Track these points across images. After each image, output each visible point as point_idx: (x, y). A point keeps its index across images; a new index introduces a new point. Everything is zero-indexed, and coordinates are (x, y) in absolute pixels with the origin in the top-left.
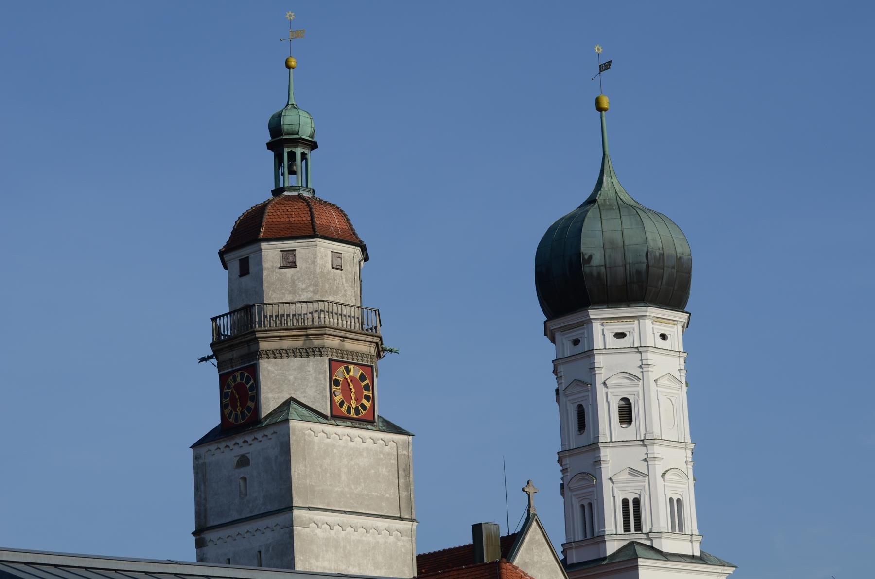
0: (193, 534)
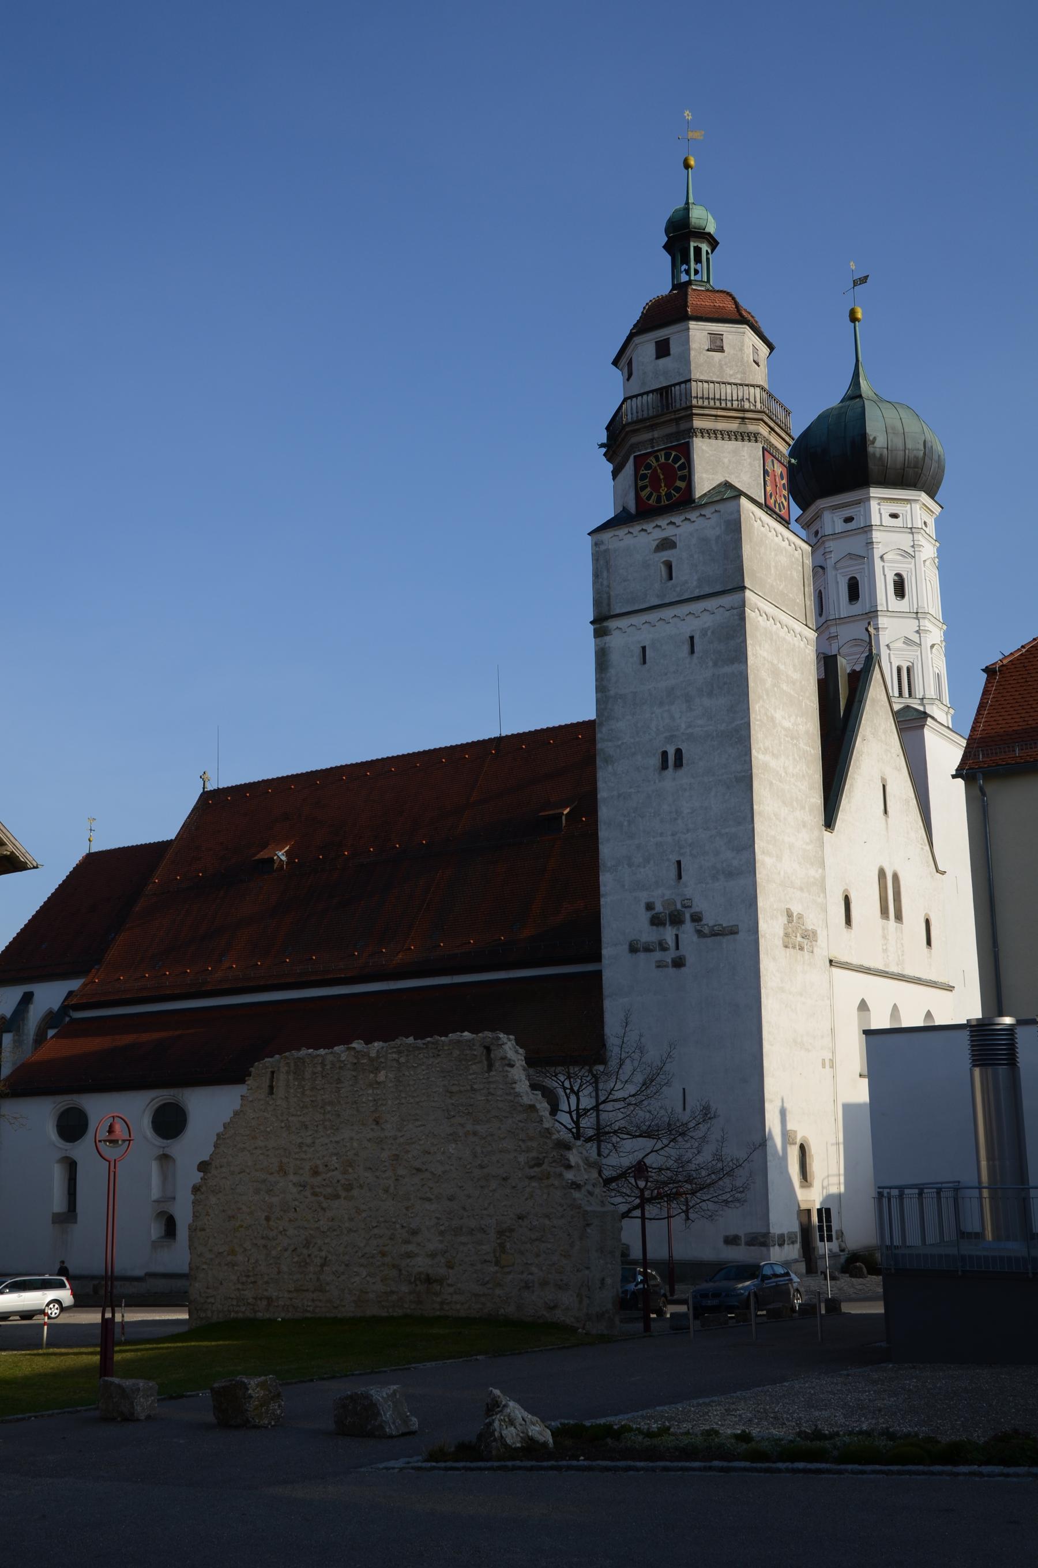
0: (591, 623)
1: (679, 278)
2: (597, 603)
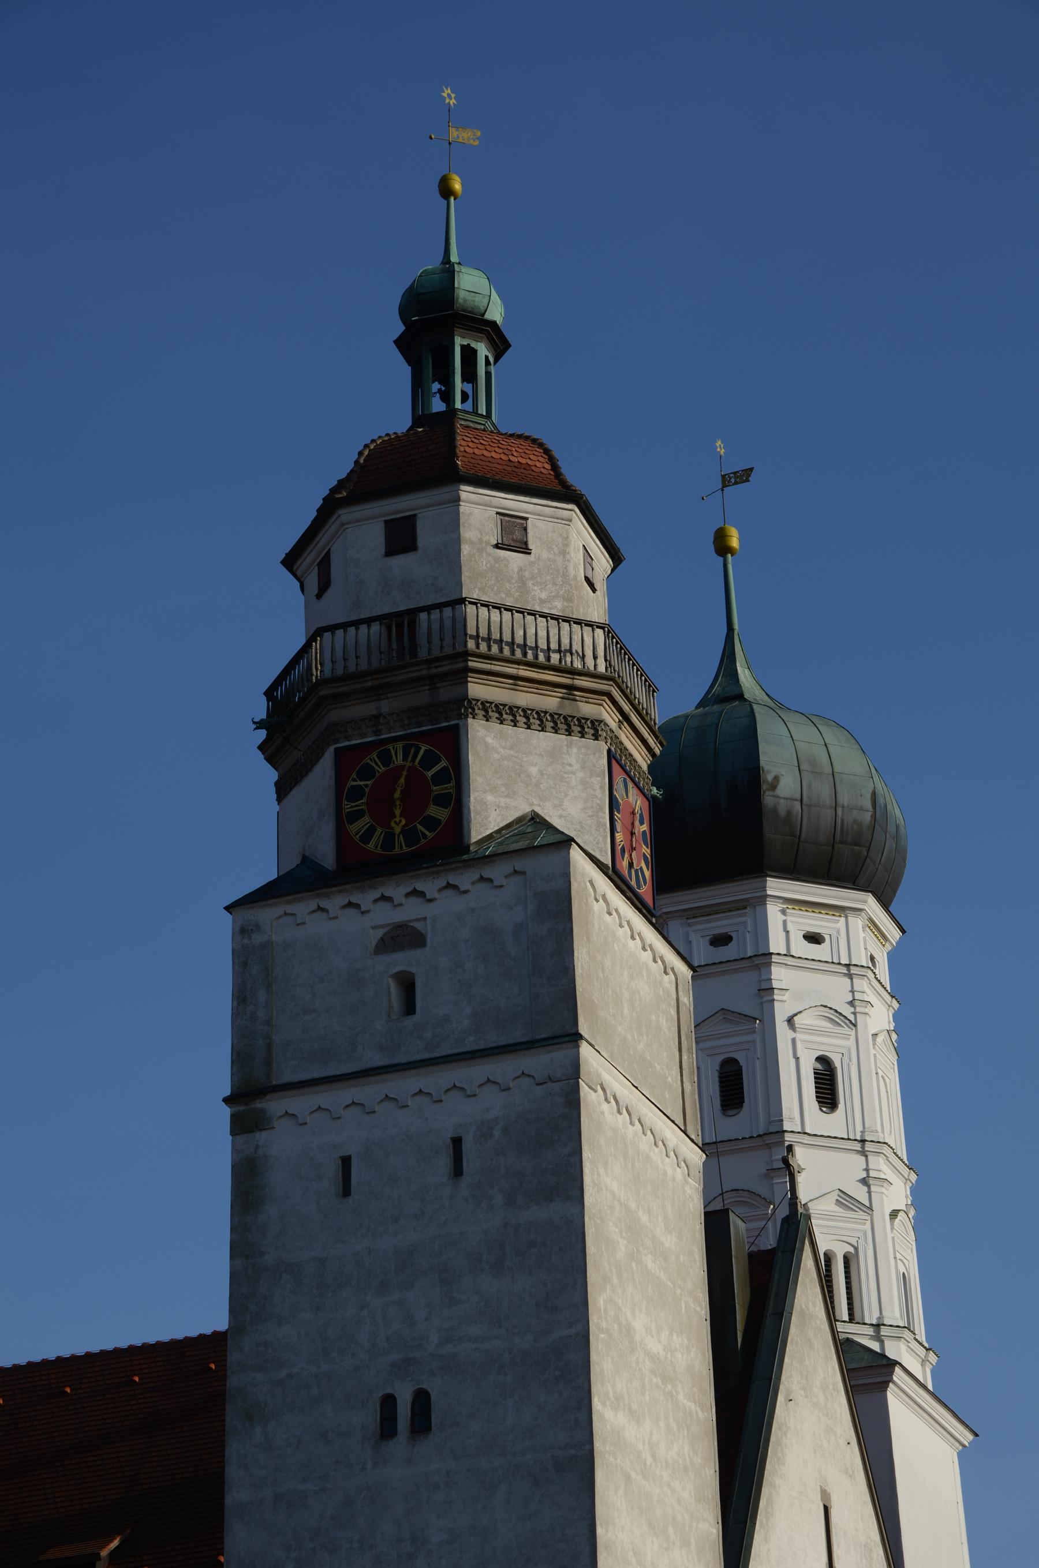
0: (226, 1100)
1: (426, 404)
2: (241, 1058)
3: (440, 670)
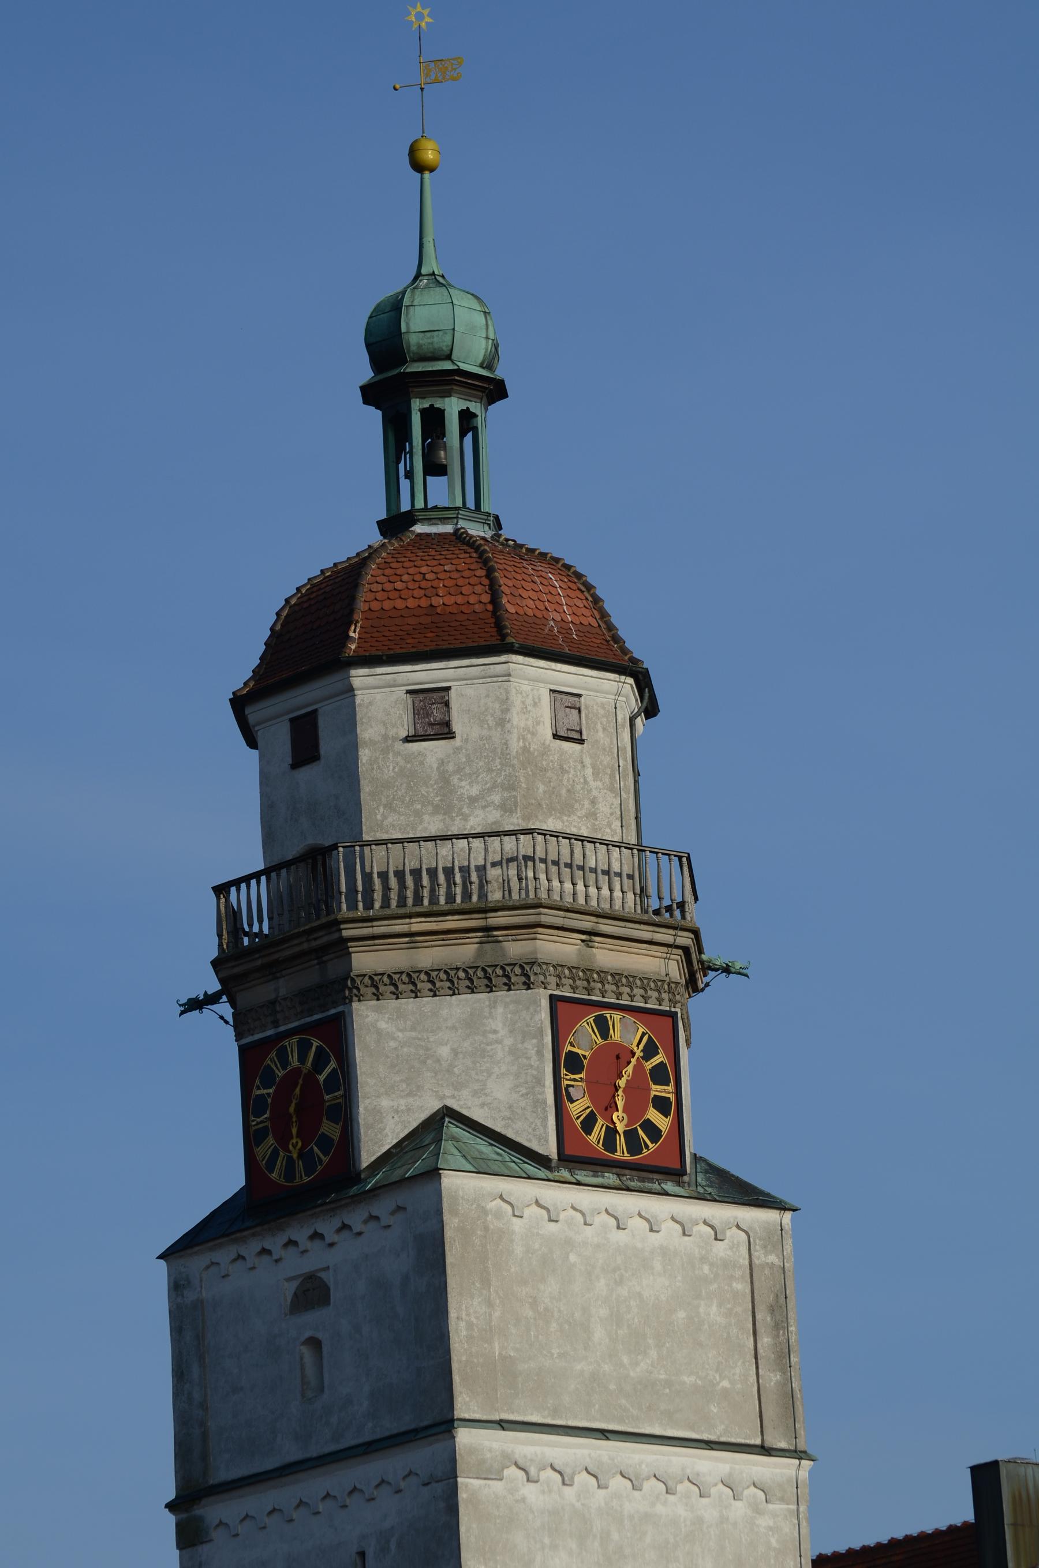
3: (319, 942)
